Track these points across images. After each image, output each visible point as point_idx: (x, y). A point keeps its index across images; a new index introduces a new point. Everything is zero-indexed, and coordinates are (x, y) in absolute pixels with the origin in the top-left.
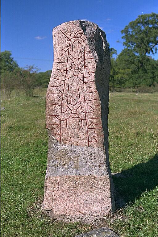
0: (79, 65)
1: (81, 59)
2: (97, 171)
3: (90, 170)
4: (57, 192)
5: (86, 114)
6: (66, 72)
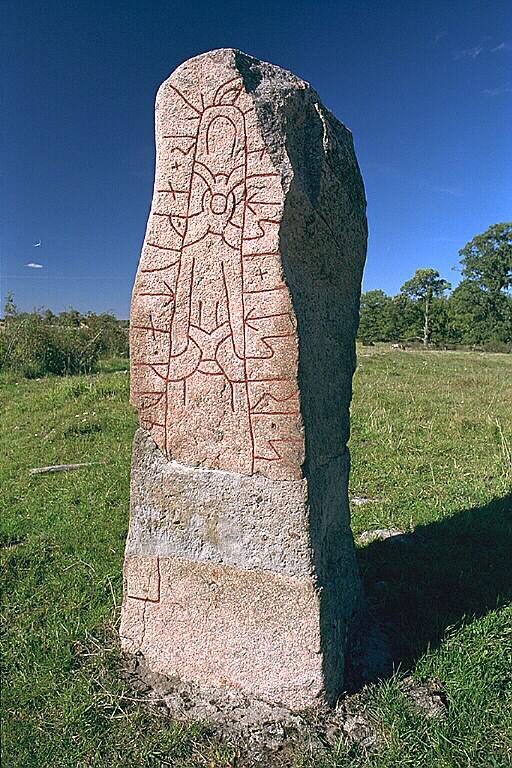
0: (227, 198)
1: (235, 178)
2: (277, 558)
3: (255, 552)
4: (155, 604)
5: (247, 365)
6: (187, 221)
